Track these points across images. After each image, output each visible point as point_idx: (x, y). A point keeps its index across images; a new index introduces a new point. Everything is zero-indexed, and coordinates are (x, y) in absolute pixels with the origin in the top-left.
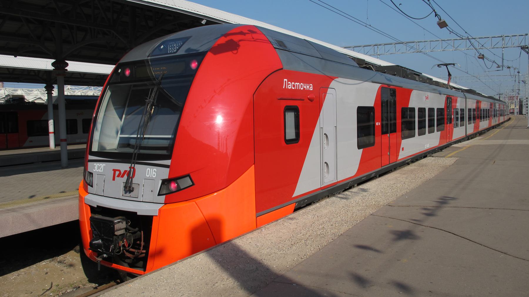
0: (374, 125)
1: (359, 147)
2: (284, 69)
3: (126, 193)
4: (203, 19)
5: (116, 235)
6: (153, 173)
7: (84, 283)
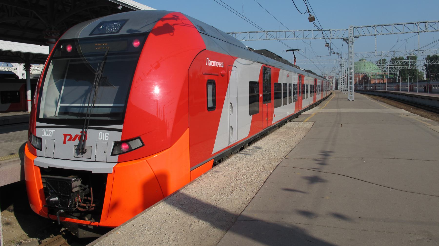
0: (259, 95)
1: (250, 115)
2: (207, 49)
3: (78, 154)
4: (119, 5)
5: (73, 192)
7: (25, 238)
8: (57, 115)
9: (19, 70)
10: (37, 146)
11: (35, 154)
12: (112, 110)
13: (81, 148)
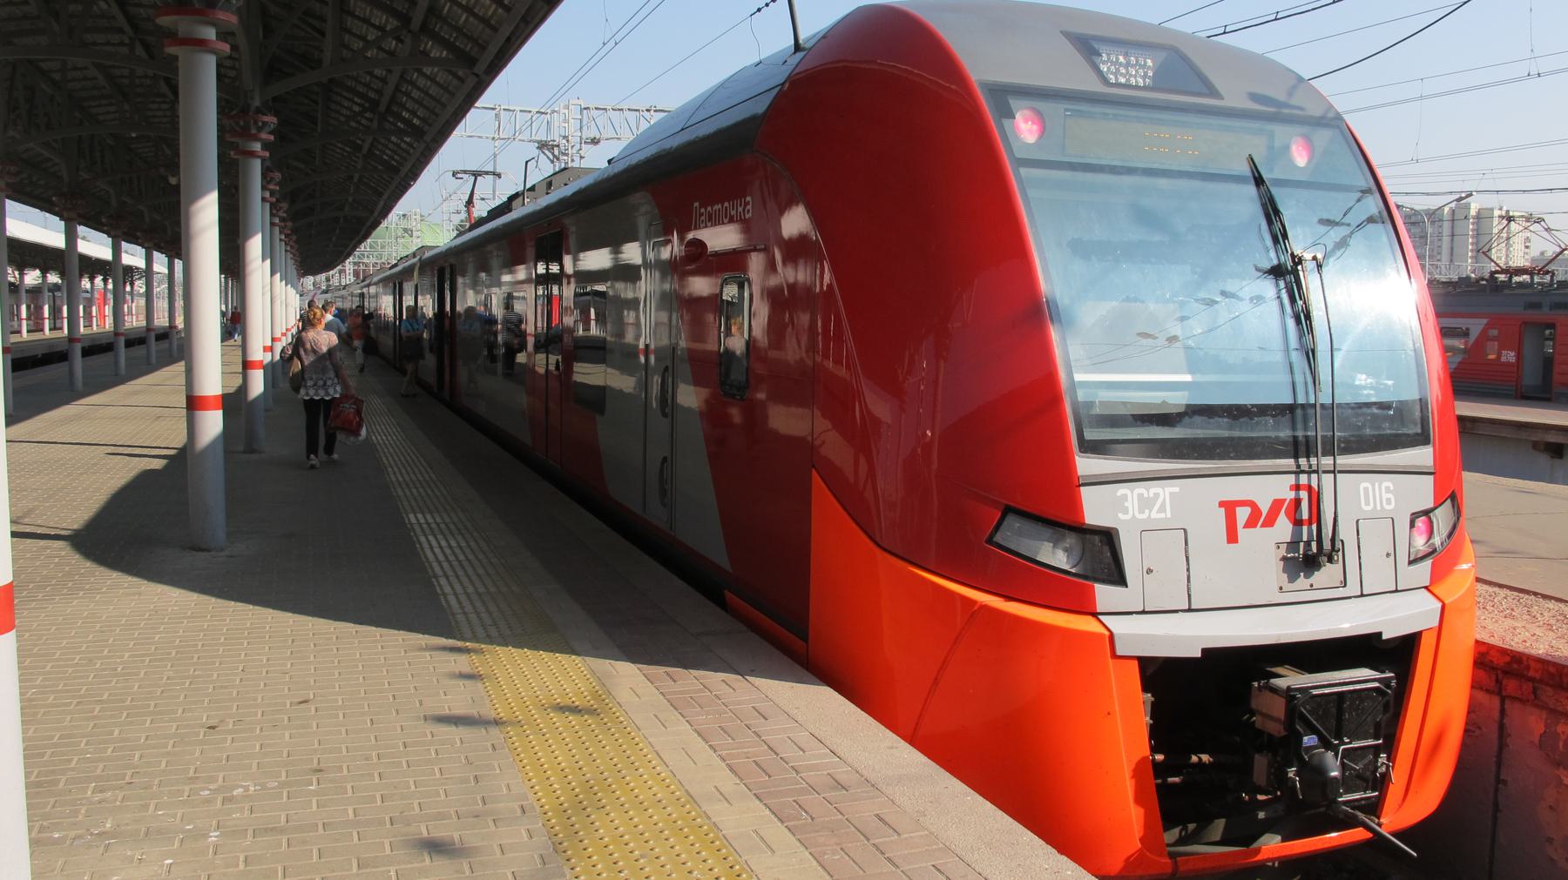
6: (1385, 496)
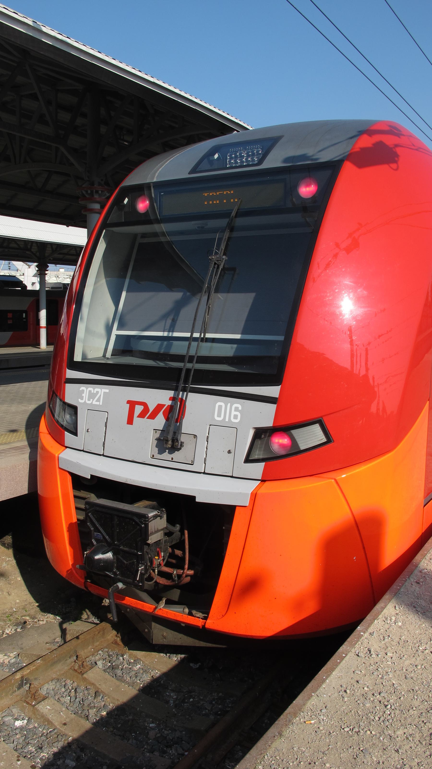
3: (161, 452)
5: (148, 545)
6: (234, 413)
7: (32, 612)
8: (109, 354)
9: (26, 274)
10: (65, 424)
11: (61, 442)
12: (237, 349)
13: (170, 437)
